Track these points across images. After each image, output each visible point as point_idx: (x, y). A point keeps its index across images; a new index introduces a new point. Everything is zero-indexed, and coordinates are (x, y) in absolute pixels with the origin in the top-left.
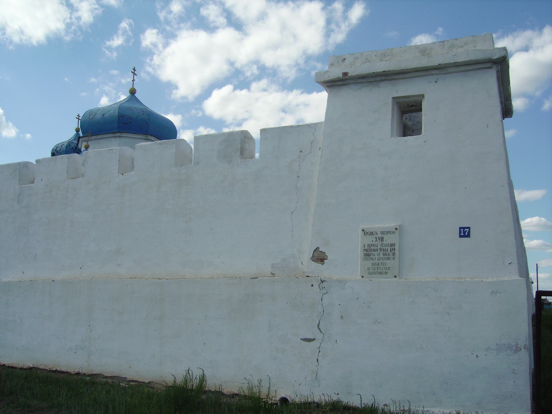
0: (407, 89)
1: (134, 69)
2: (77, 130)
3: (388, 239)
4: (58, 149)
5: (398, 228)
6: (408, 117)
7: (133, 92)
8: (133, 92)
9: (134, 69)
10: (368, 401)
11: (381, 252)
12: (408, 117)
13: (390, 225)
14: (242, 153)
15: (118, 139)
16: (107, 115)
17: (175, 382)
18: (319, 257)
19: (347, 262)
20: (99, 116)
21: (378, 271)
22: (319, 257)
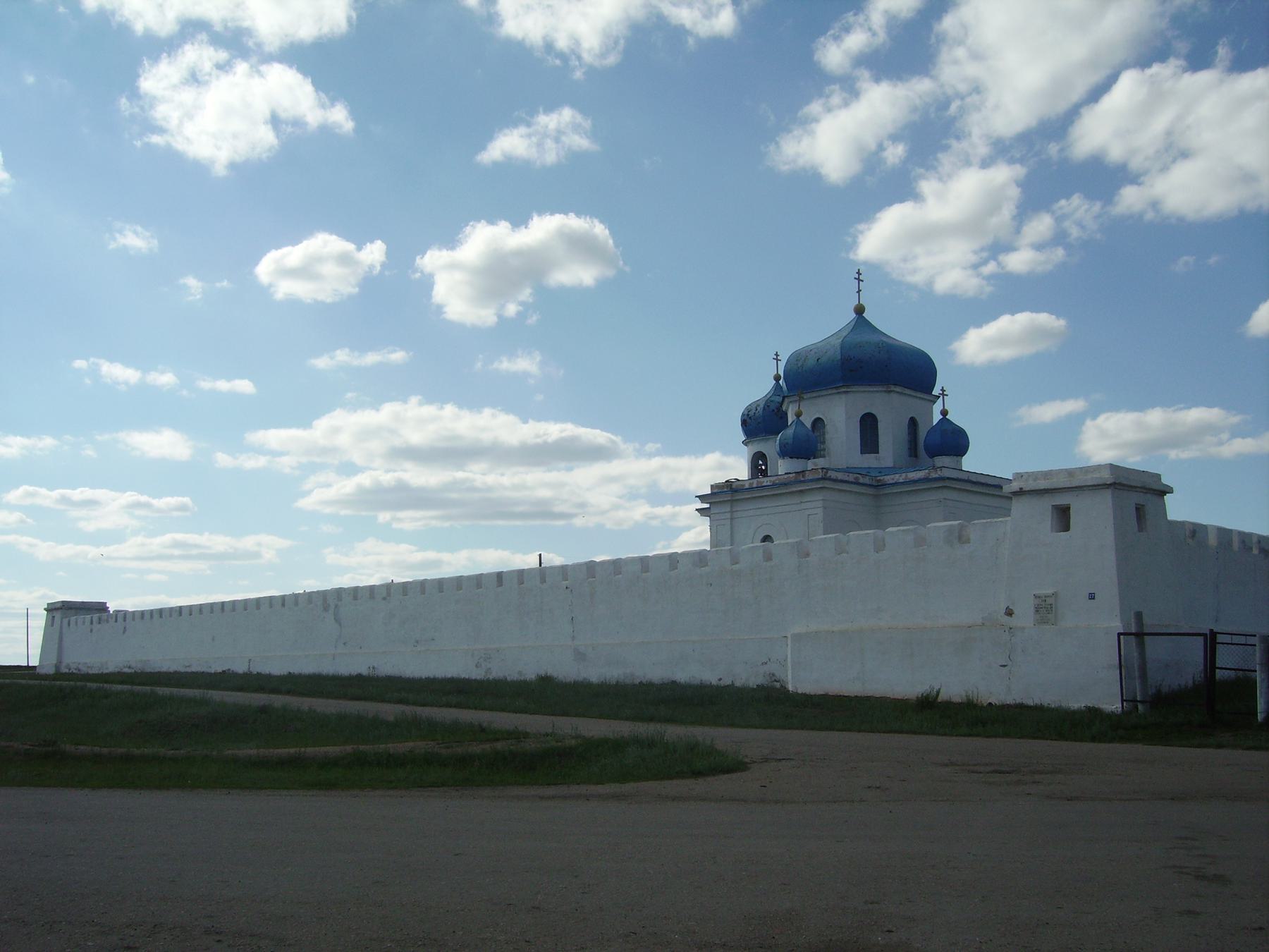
0: (1061, 500)
1: (859, 273)
2: (777, 378)
3: (1049, 601)
4: (751, 413)
5: (1012, 622)
6: (1063, 517)
7: (860, 310)
8: (860, 310)
9: (859, 273)
10: (1037, 701)
11: (1045, 609)
12: (1063, 517)
13: (1050, 591)
14: (960, 538)
15: (843, 396)
16: (823, 360)
17: (60, 662)
18: (1009, 613)
19: (1025, 617)
20: (811, 362)
21: (1042, 621)
22: (1009, 613)
